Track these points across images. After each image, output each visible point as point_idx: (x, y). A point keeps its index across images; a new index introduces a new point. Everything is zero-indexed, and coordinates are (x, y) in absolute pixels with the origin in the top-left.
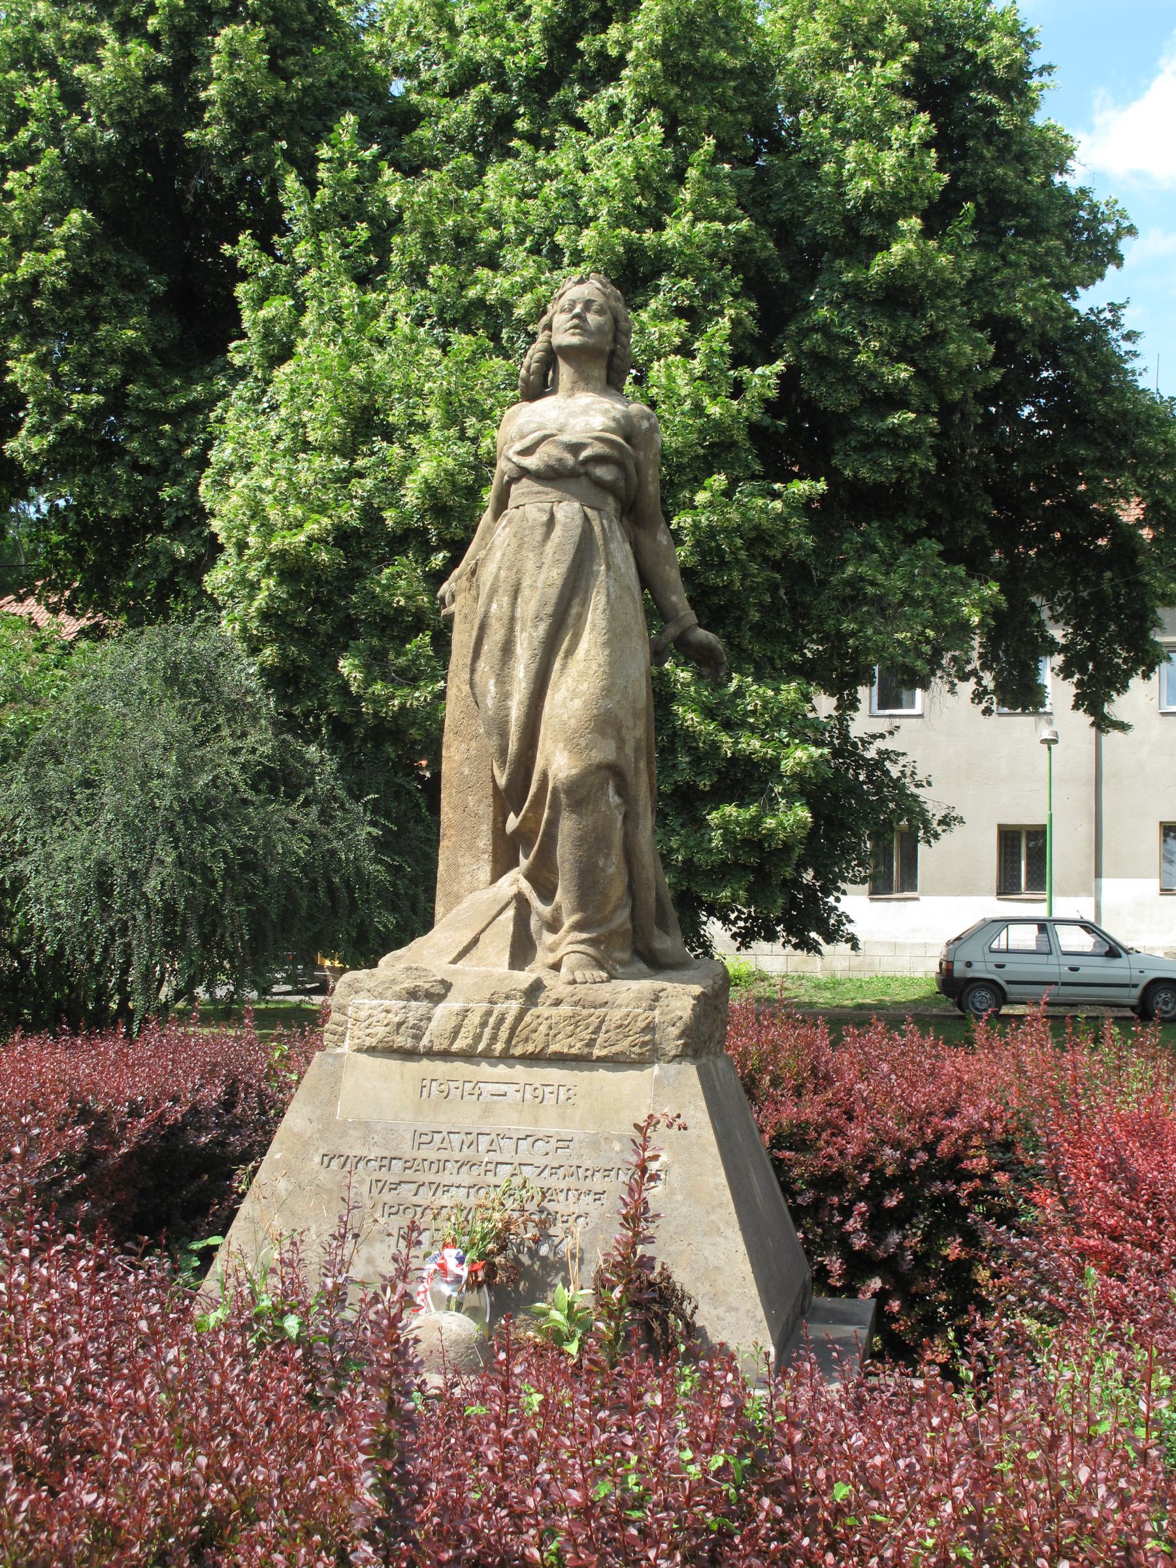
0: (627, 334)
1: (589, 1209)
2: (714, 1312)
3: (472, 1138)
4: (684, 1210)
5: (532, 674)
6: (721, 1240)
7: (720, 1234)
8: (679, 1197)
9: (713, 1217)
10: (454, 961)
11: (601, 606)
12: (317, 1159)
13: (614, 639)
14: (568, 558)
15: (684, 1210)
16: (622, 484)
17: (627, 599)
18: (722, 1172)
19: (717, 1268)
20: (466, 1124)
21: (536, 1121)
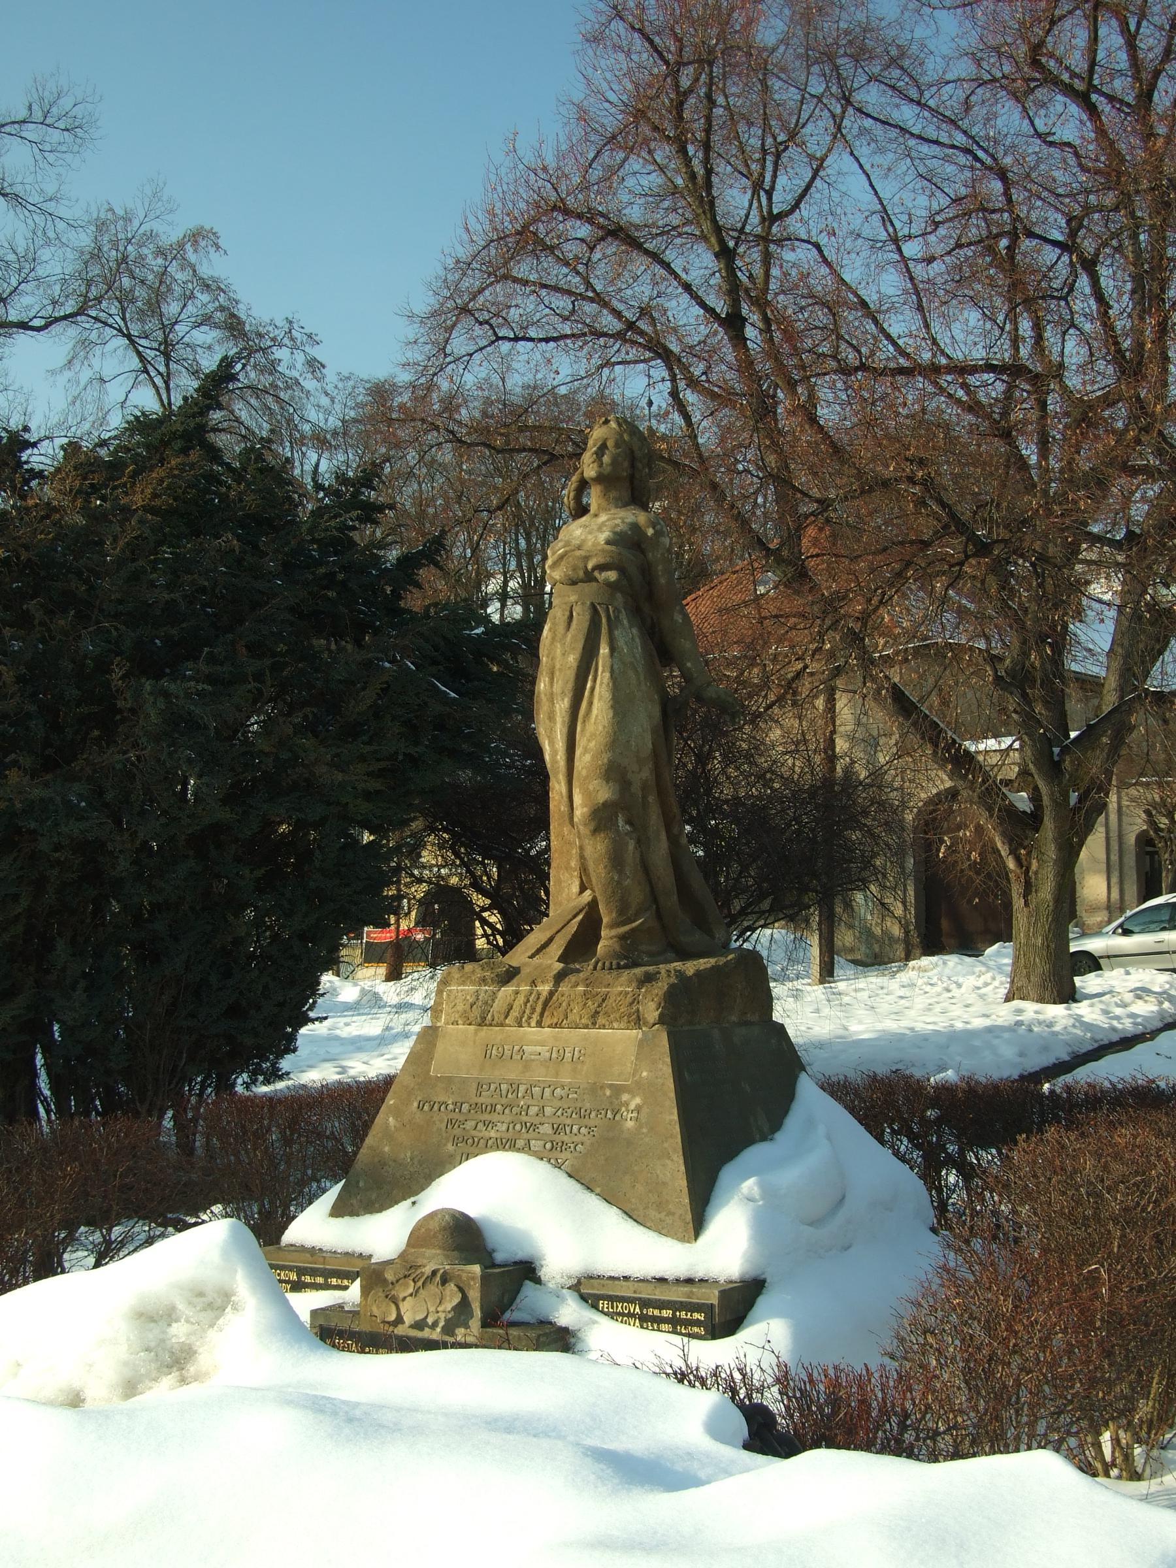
0: (1133, 292)
1: (585, 1139)
2: (658, 1216)
3: (514, 1087)
4: (647, 1140)
5: (565, 736)
6: (668, 1162)
7: (669, 1158)
8: (645, 1130)
9: (666, 1145)
10: (532, 957)
11: (606, 681)
12: (416, 1104)
13: (620, 705)
14: (580, 646)
15: (647, 1140)
16: (625, 582)
17: (631, 673)
18: (675, 1111)
19: (664, 1183)
20: (512, 1076)
21: (557, 1075)
